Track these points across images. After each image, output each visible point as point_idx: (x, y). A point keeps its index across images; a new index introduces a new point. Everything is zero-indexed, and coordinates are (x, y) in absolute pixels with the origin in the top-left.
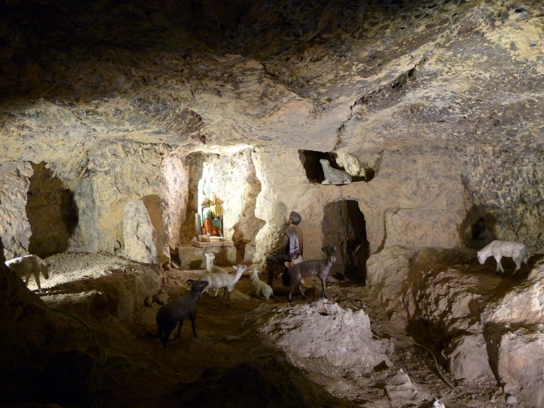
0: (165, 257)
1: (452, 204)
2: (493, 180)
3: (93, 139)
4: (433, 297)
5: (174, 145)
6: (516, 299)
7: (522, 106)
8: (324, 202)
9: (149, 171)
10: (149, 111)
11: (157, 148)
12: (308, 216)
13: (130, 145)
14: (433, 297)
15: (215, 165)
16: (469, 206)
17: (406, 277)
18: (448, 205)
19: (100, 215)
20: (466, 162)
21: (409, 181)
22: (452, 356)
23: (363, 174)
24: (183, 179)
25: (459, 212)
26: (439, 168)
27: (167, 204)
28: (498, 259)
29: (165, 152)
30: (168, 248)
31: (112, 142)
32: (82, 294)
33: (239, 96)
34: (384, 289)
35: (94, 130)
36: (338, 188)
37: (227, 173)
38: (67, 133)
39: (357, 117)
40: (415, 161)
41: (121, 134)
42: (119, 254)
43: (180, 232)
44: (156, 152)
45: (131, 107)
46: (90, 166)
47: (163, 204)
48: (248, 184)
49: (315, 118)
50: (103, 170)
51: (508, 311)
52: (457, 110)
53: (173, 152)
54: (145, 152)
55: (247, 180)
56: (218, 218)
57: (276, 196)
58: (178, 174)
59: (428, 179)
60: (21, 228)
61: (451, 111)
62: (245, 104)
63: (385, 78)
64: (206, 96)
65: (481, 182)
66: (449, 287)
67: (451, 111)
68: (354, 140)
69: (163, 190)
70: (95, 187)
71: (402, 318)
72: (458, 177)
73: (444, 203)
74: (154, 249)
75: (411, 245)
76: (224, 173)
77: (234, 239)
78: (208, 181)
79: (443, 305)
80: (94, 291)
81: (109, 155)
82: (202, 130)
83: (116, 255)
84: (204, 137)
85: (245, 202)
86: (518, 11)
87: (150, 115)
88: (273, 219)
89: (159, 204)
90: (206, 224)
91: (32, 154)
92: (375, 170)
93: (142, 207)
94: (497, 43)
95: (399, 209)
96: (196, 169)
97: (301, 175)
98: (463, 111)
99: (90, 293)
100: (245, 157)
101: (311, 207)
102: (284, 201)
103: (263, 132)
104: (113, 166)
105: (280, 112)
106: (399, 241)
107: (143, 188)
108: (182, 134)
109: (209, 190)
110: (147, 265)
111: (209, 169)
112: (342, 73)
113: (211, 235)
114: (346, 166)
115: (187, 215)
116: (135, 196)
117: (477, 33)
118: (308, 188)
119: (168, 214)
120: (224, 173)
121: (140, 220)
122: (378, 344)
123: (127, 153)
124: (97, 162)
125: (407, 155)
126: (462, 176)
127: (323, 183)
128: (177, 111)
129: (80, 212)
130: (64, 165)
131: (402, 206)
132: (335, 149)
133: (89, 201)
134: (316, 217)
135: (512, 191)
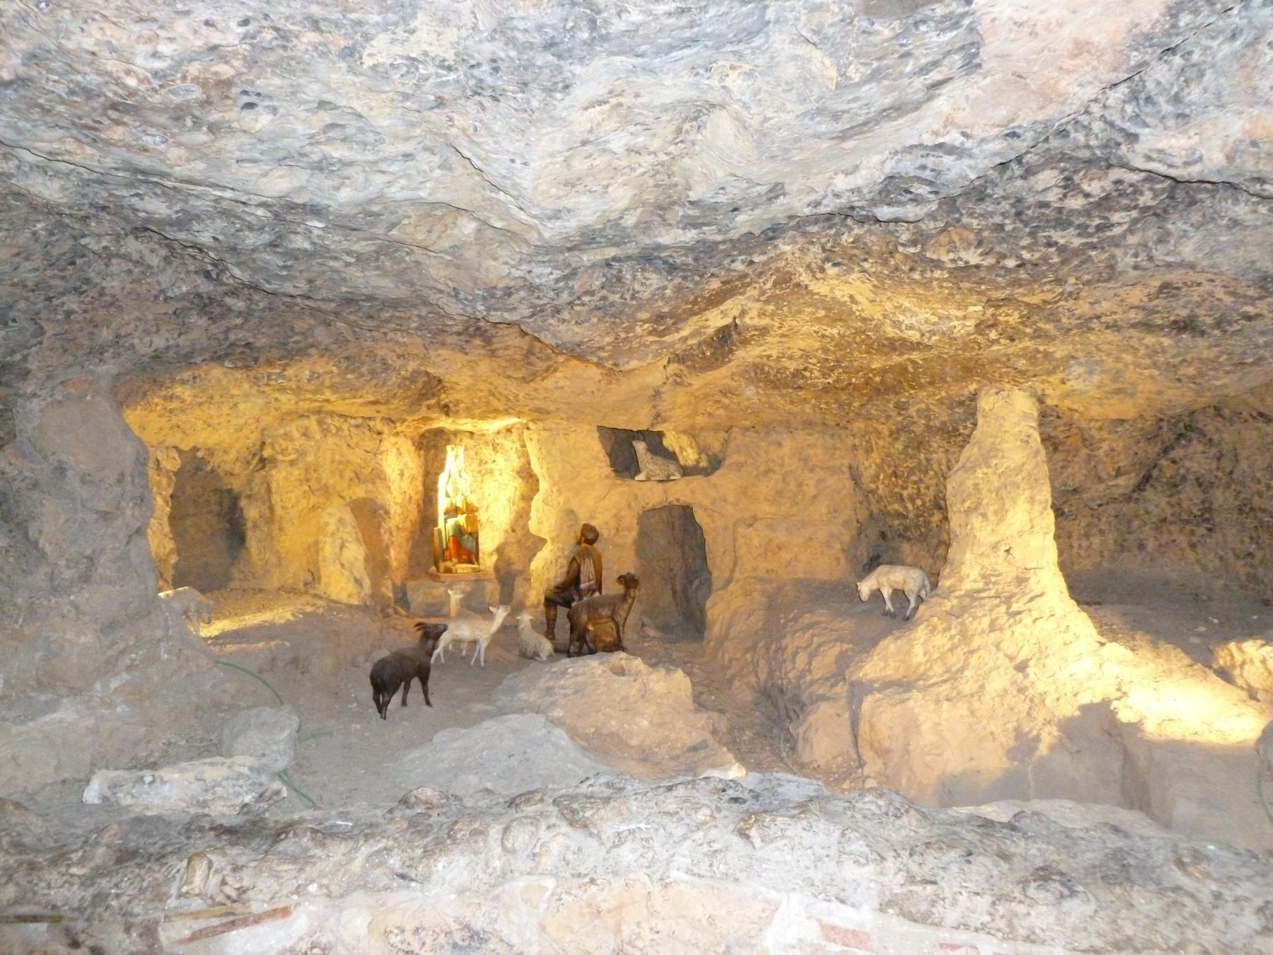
0: (383, 596)
1: (836, 511)
2: (895, 474)
3: (273, 412)
4: (790, 650)
5: (399, 420)
6: (892, 647)
7: (902, 369)
8: (637, 508)
10: (362, 375)
11: (372, 423)
12: (613, 532)
13: (329, 420)
14: (790, 650)
15: (466, 449)
16: (863, 515)
17: (760, 625)
18: (829, 512)
19: (281, 529)
20: (855, 446)
21: (771, 475)
22: (801, 730)
23: (704, 464)
24: (414, 471)
25: (846, 524)
26: (817, 454)
27: (387, 513)
28: (886, 593)
29: (386, 429)
30: (389, 583)
31: (302, 416)
32: (261, 645)
33: (493, 354)
34: (726, 644)
35: (276, 399)
36: (660, 486)
38: (236, 405)
39: (675, 381)
40: (780, 444)
41: (317, 404)
42: (312, 592)
43: (410, 558)
44: (370, 429)
45: (335, 369)
46: (267, 453)
47: (382, 512)
48: (520, 480)
49: (610, 383)
50: (287, 459)
51: (882, 664)
52: (817, 373)
53: (399, 429)
54: (353, 429)
55: (518, 473)
56: (470, 534)
57: (561, 500)
58: (406, 464)
59: (799, 472)
60: (162, 550)
61: (807, 374)
62: (504, 363)
63: (693, 335)
64: (445, 353)
65: (877, 477)
66: (813, 635)
67: (807, 374)
68: (678, 412)
70: (274, 486)
71: (749, 685)
72: (845, 469)
73: (824, 510)
74: (367, 583)
75: (773, 576)
76: (481, 462)
77: (497, 569)
78: (455, 475)
79: (801, 661)
80: (278, 641)
81: (296, 434)
82: (443, 396)
83: (306, 593)
84: (446, 406)
85: (515, 508)
86: (835, 265)
87: (362, 380)
88: (558, 536)
90: (451, 545)
91: (179, 436)
92: (721, 456)
93: (348, 516)
94: (830, 295)
95: (755, 518)
96: (436, 456)
97: (603, 467)
98: (824, 375)
99: (273, 644)
100: (514, 436)
101: (617, 517)
102: (574, 506)
103: (536, 402)
104: (302, 453)
105: (558, 374)
106: (755, 569)
107: (349, 486)
108: (412, 404)
109: (456, 490)
110: (357, 607)
111: (456, 457)
112: (623, 335)
113: (460, 562)
114: (677, 451)
115: (421, 531)
116: (336, 500)
117: (798, 285)
118: (613, 486)
120: (481, 462)
121: (345, 536)
122: (702, 719)
123: (326, 431)
124: (277, 446)
125: (767, 433)
126: (850, 467)
127: (637, 478)
128: (403, 373)
129: (249, 524)
130: (225, 452)
131: (760, 515)
132: (653, 425)
133: (264, 509)
134: (626, 533)
135: (922, 491)
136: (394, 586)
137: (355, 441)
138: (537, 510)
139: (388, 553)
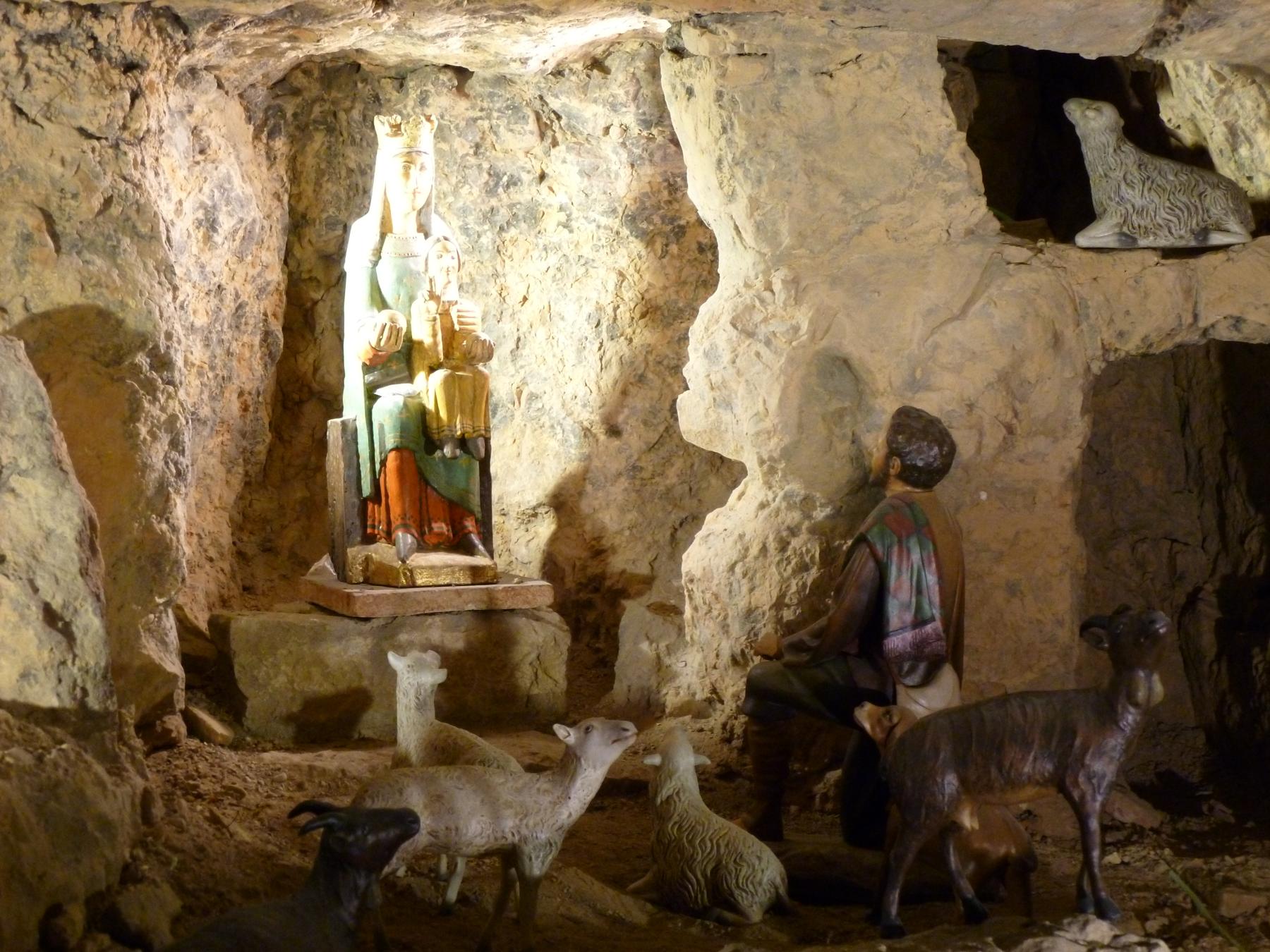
5: (203, 16)
9: (57, 169)
11: (103, 29)
12: (993, 438)
24: (254, 213)
27: (162, 363)
29: (155, 53)
30: (170, 622)
36: (1171, 272)
37: (513, 182)
43: (238, 528)
44: (97, 52)
47: (142, 359)
48: (637, 246)
53: (199, 56)
54: (36, 53)
55: (631, 219)
56: (463, 443)
69: (142, 279)
74: (89, 623)
76: (497, 181)
77: (551, 567)
78: (404, 224)
85: (614, 349)
89: (118, 361)
96: (331, 155)
100: (619, 84)
109: (407, 278)
110: (53, 716)
111: (410, 157)
113: (422, 547)
114: (1216, 142)
115: (275, 427)
118: (992, 270)
119: (173, 419)
120: (497, 181)
127: (1082, 239)
134: (1040, 443)
136: (185, 627)
137: (41, 93)
138: (711, 355)
139: (164, 512)
